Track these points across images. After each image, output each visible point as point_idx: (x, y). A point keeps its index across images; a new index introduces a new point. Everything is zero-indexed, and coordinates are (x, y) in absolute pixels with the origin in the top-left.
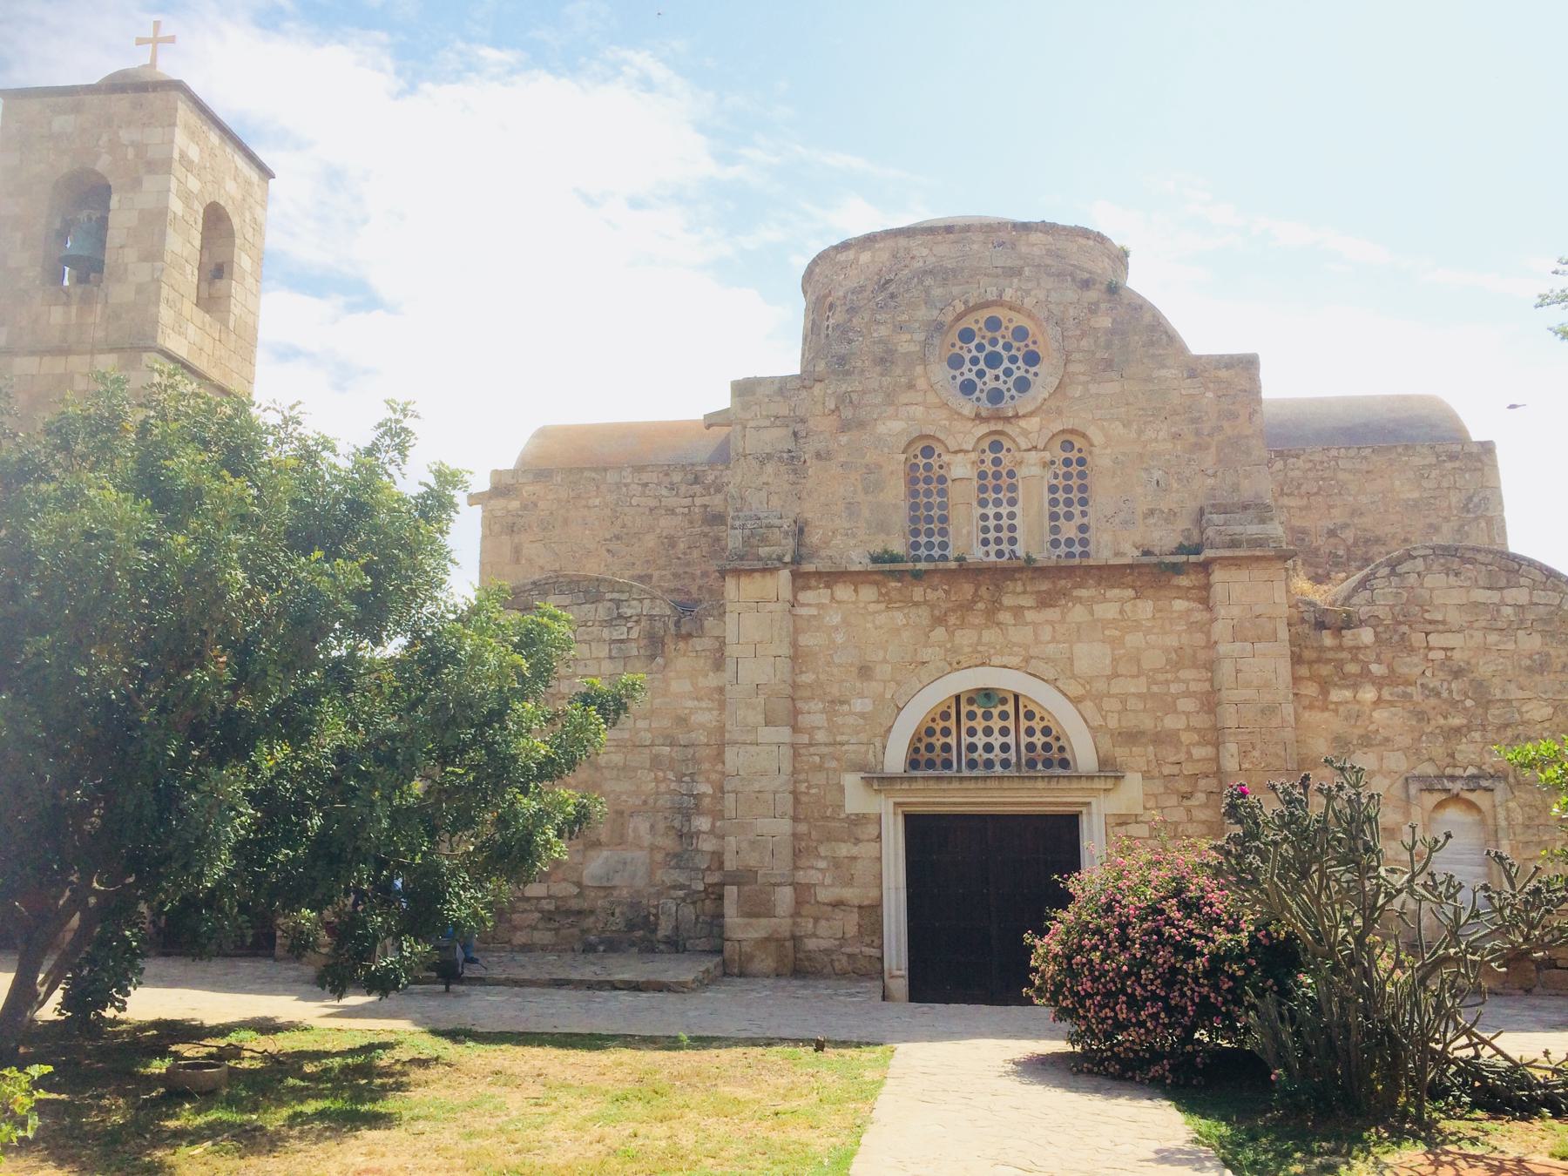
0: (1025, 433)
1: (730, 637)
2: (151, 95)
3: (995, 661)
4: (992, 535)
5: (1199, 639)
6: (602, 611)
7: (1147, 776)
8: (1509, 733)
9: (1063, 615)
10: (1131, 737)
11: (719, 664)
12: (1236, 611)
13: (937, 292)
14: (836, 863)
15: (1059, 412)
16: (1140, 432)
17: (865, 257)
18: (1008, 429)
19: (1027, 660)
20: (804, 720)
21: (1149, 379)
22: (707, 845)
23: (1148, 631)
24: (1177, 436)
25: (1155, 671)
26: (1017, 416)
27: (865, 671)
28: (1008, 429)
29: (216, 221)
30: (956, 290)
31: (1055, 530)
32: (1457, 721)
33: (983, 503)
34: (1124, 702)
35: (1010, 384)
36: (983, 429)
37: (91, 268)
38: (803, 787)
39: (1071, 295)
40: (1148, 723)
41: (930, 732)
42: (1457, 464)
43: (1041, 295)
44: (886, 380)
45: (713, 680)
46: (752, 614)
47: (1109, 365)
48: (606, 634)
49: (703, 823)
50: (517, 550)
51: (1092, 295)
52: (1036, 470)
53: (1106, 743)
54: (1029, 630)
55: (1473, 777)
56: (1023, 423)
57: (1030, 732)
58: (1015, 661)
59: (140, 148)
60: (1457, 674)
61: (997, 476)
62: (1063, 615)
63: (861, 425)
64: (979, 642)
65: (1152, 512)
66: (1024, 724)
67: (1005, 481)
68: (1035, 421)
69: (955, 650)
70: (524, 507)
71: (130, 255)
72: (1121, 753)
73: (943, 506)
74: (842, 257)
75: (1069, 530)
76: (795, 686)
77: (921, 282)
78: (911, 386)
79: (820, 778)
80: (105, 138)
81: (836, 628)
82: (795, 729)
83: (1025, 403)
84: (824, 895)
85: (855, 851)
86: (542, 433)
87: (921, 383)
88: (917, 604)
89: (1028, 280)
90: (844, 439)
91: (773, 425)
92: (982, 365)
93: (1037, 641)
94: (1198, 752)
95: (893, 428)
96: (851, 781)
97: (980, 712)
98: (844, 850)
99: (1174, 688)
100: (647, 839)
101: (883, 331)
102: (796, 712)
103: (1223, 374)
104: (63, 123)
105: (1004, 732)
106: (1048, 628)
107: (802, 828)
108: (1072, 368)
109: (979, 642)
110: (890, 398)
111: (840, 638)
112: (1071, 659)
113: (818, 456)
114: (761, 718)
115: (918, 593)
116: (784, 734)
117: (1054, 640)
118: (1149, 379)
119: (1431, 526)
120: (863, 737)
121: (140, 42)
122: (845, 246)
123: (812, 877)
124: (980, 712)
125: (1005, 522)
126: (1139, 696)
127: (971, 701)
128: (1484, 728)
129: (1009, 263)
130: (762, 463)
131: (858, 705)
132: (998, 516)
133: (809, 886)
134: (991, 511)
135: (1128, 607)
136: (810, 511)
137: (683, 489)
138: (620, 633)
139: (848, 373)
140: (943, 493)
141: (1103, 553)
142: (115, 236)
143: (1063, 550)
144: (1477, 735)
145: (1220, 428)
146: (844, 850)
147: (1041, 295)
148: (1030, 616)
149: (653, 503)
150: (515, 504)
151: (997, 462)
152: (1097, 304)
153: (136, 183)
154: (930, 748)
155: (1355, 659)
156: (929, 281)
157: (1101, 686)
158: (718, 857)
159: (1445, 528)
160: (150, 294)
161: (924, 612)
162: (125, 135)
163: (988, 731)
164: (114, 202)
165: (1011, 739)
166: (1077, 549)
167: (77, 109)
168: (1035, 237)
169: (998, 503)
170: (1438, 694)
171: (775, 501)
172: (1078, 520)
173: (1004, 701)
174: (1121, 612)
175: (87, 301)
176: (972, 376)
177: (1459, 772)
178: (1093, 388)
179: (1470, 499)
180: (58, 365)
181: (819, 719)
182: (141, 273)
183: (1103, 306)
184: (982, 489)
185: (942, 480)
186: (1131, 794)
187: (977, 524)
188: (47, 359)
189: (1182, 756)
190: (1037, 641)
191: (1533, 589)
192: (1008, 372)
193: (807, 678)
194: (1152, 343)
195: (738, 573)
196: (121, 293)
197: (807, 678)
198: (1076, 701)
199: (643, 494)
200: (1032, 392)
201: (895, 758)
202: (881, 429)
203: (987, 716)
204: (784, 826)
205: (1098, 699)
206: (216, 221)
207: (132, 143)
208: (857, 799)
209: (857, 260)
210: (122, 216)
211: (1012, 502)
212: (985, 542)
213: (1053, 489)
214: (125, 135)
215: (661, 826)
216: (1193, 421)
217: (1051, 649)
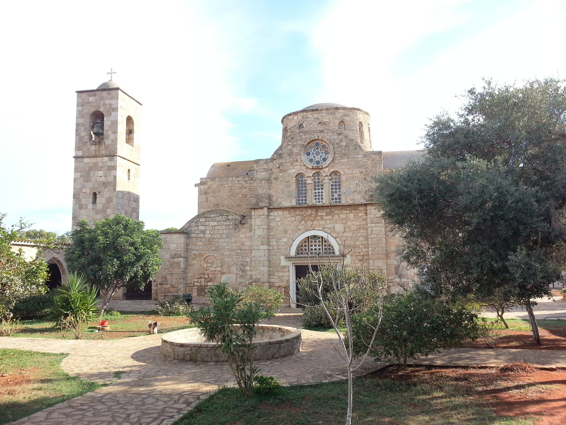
0: (325, 172)
1: (253, 224)
2: (112, 91)
3: (316, 229)
4: (317, 197)
5: (364, 222)
6: (224, 218)
9: (333, 217)
11: (251, 231)
12: (372, 216)
13: (303, 137)
14: (279, 277)
15: (333, 167)
16: (352, 172)
17: (295, 117)
18: (320, 171)
19: (324, 228)
20: (271, 244)
21: (355, 158)
22: (249, 273)
23: (353, 221)
24: (361, 172)
27: (286, 232)
28: (320, 171)
29: (129, 120)
30: (308, 136)
31: (333, 196)
33: (315, 189)
36: (314, 171)
37: (99, 135)
38: (271, 259)
39: (336, 137)
40: (352, 243)
41: (302, 246)
43: (328, 137)
44: (291, 160)
45: (250, 234)
46: (258, 220)
47: (345, 154)
48: (225, 223)
49: (248, 268)
50: (207, 198)
51: (341, 137)
52: (328, 181)
57: (325, 245)
58: (321, 229)
59: (110, 105)
61: (319, 182)
62: (333, 217)
63: (285, 171)
64: (312, 224)
65: (355, 191)
66: (324, 243)
67: (321, 183)
68: (327, 169)
73: (306, 190)
74: (290, 117)
75: (336, 196)
76: (269, 235)
78: (297, 161)
79: (275, 257)
80: (102, 103)
81: (278, 221)
82: (269, 245)
83: (325, 164)
84: (277, 285)
85: (283, 274)
86: (213, 166)
87: (299, 160)
90: (281, 174)
94: (364, 250)
95: (293, 171)
96: (282, 258)
98: (281, 274)
99: (358, 235)
100: (235, 272)
101: (290, 147)
102: (269, 242)
103: (373, 156)
104: (91, 99)
105: (319, 246)
107: (271, 269)
108: (336, 156)
109: (312, 224)
110: (292, 164)
111: (279, 224)
112: (334, 228)
113: (275, 179)
114: (260, 244)
115: (298, 213)
116: (266, 247)
118: (355, 158)
120: (285, 247)
121: (108, 73)
122: (290, 115)
123: (274, 280)
125: (320, 194)
126: (350, 237)
127: (311, 238)
130: (261, 180)
131: (284, 240)
132: (319, 193)
133: (273, 282)
134: (317, 191)
135: (348, 215)
136: (273, 192)
137: (248, 181)
138: (228, 223)
139: (282, 158)
140: (306, 187)
141: (343, 202)
142: (106, 127)
143: (334, 201)
146: (281, 274)
147: (328, 137)
148: (324, 218)
149: (241, 186)
150: (206, 187)
151: (318, 179)
153: (110, 115)
154: (302, 250)
156: (301, 134)
157: (341, 234)
158: (251, 275)
160: (115, 141)
161: (299, 217)
162: (107, 102)
163: (315, 246)
164: (105, 119)
166: (338, 200)
167: (95, 95)
168: (340, 111)
169: (319, 189)
171: (264, 190)
172: (338, 193)
173: (319, 238)
176: (312, 158)
178: (341, 161)
180: (94, 160)
181: (275, 243)
182: (112, 137)
183: (344, 139)
184: (315, 186)
185: (305, 183)
187: (313, 194)
189: (360, 251)
193: (272, 233)
195: (254, 209)
196: (108, 142)
197: (272, 233)
198: (335, 238)
199: (238, 184)
200: (327, 161)
201: (293, 253)
202: (290, 172)
203: (315, 242)
204: (266, 269)
205: (340, 237)
206: (129, 120)
207: (108, 104)
208: (284, 262)
209: (293, 118)
210: (107, 122)
211: (322, 189)
212: (316, 199)
213: (332, 185)
214: (107, 102)
215: (238, 269)
217: (329, 226)
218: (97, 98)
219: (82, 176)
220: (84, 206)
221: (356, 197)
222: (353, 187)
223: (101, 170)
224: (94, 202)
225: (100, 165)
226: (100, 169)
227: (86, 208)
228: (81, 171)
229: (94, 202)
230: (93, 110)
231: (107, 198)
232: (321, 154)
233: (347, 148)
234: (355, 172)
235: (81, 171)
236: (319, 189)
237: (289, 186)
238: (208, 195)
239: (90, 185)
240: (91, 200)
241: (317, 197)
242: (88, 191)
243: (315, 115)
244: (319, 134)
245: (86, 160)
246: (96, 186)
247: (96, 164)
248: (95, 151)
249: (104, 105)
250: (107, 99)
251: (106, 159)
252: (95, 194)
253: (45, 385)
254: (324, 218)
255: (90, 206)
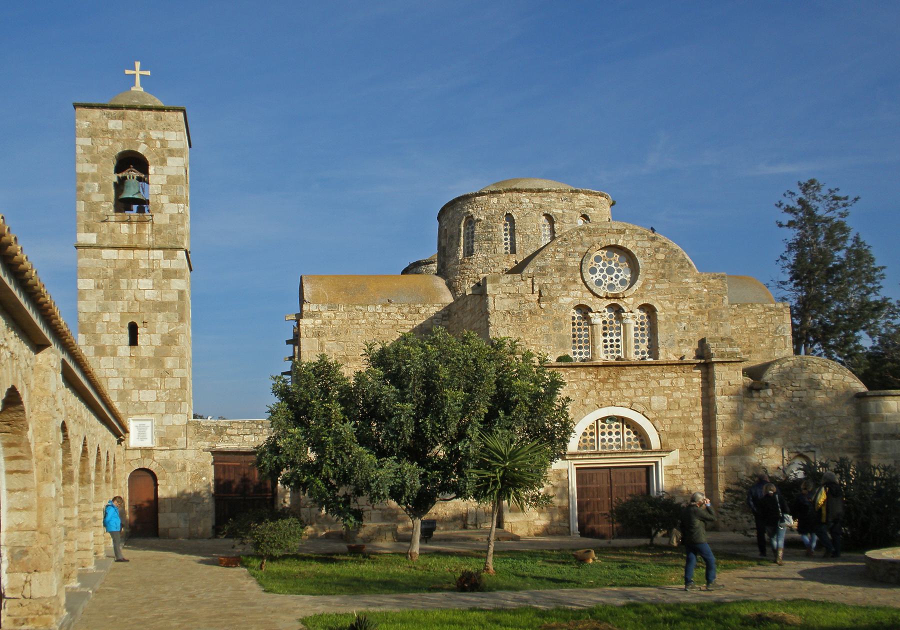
0: (627, 305)
2: (167, 113)
7: (682, 450)
8: (822, 429)
10: (675, 435)
16: (677, 306)
17: (495, 200)
23: (683, 391)
25: (686, 407)
26: (624, 297)
30: (595, 239)
32: (802, 425)
33: (605, 335)
34: (672, 421)
35: (618, 282)
39: (648, 244)
40: (682, 429)
42: (772, 313)
44: (563, 279)
47: (663, 276)
53: (664, 437)
54: (632, 391)
55: (808, 447)
56: (625, 300)
60: (804, 407)
65: (682, 340)
69: (601, 399)
70: (324, 323)
71: (164, 199)
72: (671, 442)
77: (578, 234)
78: (575, 282)
80: (142, 135)
88: (583, 380)
89: (628, 236)
91: (508, 297)
92: (605, 273)
93: (636, 396)
97: (606, 425)
101: (561, 256)
106: (640, 390)
112: (650, 404)
117: (643, 395)
118: (681, 283)
119: (761, 339)
124: (606, 425)
125: (615, 343)
128: (812, 428)
129: (619, 228)
132: (611, 341)
137: (409, 316)
139: (545, 275)
144: (809, 431)
145: (710, 306)
152: (658, 248)
153: (163, 162)
155: (765, 401)
157: (663, 414)
159: (767, 341)
162: (154, 134)
165: (594, 437)
167: (122, 117)
169: (611, 335)
170: (796, 415)
174: (672, 383)
175: (141, 222)
177: (803, 445)
178: (657, 286)
179: (777, 328)
180: (130, 255)
183: (661, 249)
186: (674, 457)
188: (122, 251)
190: (636, 396)
191: (834, 373)
192: (617, 277)
194: (682, 267)
207: (158, 139)
212: (606, 352)
214: (154, 134)
216: (698, 301)
218: (130, 124)
219: (98, 287)
220: (108, 350)
221: (683, 350)
222: (678, 334)
223: (146, 277)
224: (133, 342)
225: (143, 266)
226: (146, 274)
227: (114, 354)
228: (98, 277)
229: (133, 342)
230: (120, 148)
231: (163, 336)
232: (616, 273)
233: (667, 265)
234: (681, 306)
235: (98, 277)
236: (611, 335)
237: (560, 327)
238: (324, 339)
239: (121, 306)
240: (126, 338)
241: (609, 349)
242: (116, 319)
243: (537, 200)
244: (617, 237)
245: (107, 254)
246: (136, 308)
247: (133, 263)
248: (130, 236)
249: (148, 141)
250: (156, 128)
251: (159, 254)
252: (133, 329)
253: (747, 581)
254: (633, 385)
255: (124, 350)
